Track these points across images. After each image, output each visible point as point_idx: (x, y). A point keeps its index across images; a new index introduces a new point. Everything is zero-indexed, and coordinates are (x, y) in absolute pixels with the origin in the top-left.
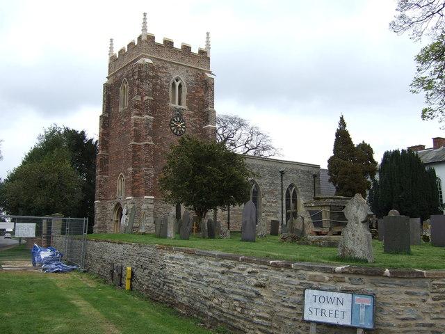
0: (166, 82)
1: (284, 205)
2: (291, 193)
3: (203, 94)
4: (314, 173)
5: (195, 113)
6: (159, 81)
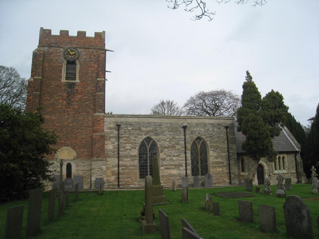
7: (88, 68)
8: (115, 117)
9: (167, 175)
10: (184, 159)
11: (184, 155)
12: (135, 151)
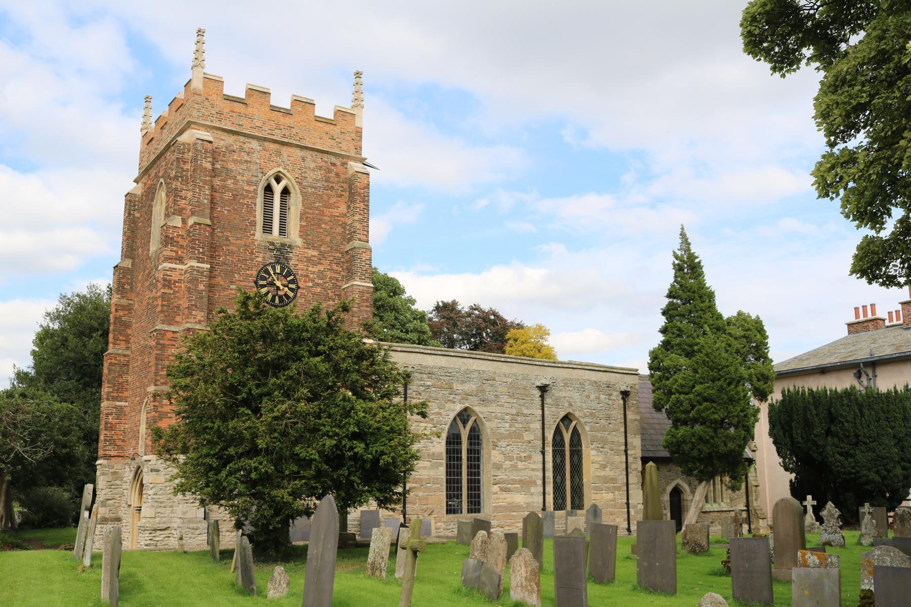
0: (249, 183)
1: (550, 465)
2: (567, 437)
3: (343, 209)
4: (623, 388)
5: (322, 255)
6: (230, 182)
7: (321, 209)
8: (397, 351)
9: (505, 507)
10: (541, 466)
11: (540, 457)
12: (440, 443)
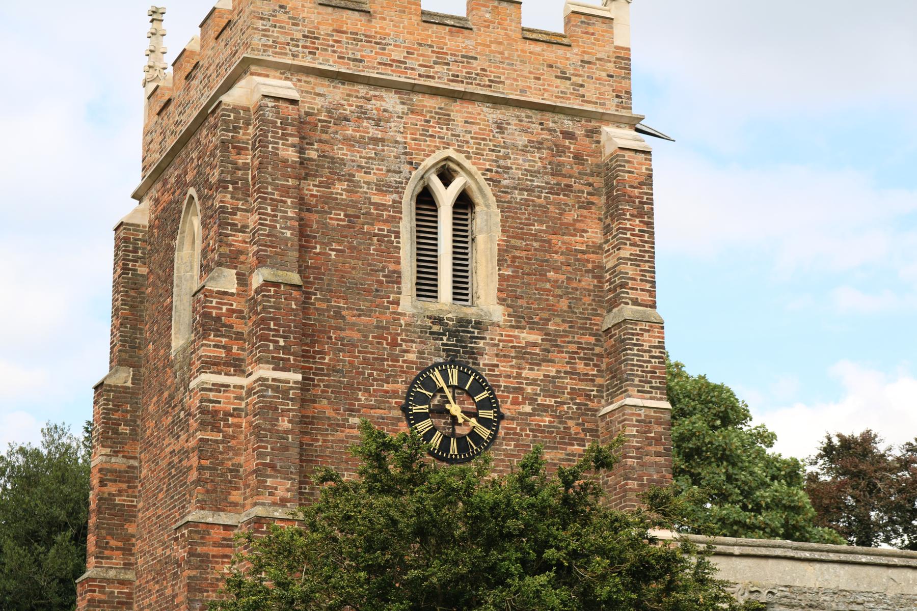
0: (383, 187)
3: (594, 234)
8: (731, 555)
